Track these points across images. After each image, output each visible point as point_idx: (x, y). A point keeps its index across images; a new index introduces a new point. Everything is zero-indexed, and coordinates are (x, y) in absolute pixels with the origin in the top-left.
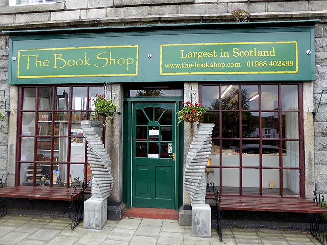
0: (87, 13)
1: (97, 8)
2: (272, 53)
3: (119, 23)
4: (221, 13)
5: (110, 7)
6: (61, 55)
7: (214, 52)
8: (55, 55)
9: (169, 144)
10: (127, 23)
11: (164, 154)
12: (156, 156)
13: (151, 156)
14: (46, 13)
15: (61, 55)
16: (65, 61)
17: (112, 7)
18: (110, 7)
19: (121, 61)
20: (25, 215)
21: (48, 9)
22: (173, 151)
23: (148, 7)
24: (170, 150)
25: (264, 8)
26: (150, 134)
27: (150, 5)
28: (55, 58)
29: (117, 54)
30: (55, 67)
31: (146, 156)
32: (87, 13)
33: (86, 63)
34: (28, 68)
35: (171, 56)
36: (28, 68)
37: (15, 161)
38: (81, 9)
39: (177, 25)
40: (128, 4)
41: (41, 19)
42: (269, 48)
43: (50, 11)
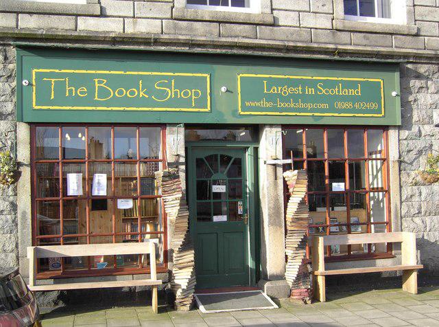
0: (135, 23)
1: (148, 18)
2: (358, 92)
3: (184, 44)
4: (336, 44)
5: (166, 19)
6: (105, 81)
7: (300, 88)
8: (96, 80)
9: (239, 203)
10: (199, 45)
11: (233, 214)
12: (224, 218)
13: (216, 219)
14: (70, 17)
15: (105, 81)
16: (168, 89)
17: (168, 19)
18: (166, 19)
19: (186, 94)
20: (362, 175)
21: (75, 12)
22: (245, 211)
23: (218, 24)
24: (240, 211)
25: (250, 34)
26: (214, 191)
27: (220, 22)
28: (97, 85)
29: (181, 83)
30: (96, 98)
31: (211, 220)
32: (135, 23)
33: (141, 93)
34: (52, 97)
35: (252, 92)
36: (52, 97)
37: (30, 237)
38: (124, 17)
39: (52, 44)
40: (192, 18)
41: (62, 25)
42: (353, 85)
43: (77, 15)
